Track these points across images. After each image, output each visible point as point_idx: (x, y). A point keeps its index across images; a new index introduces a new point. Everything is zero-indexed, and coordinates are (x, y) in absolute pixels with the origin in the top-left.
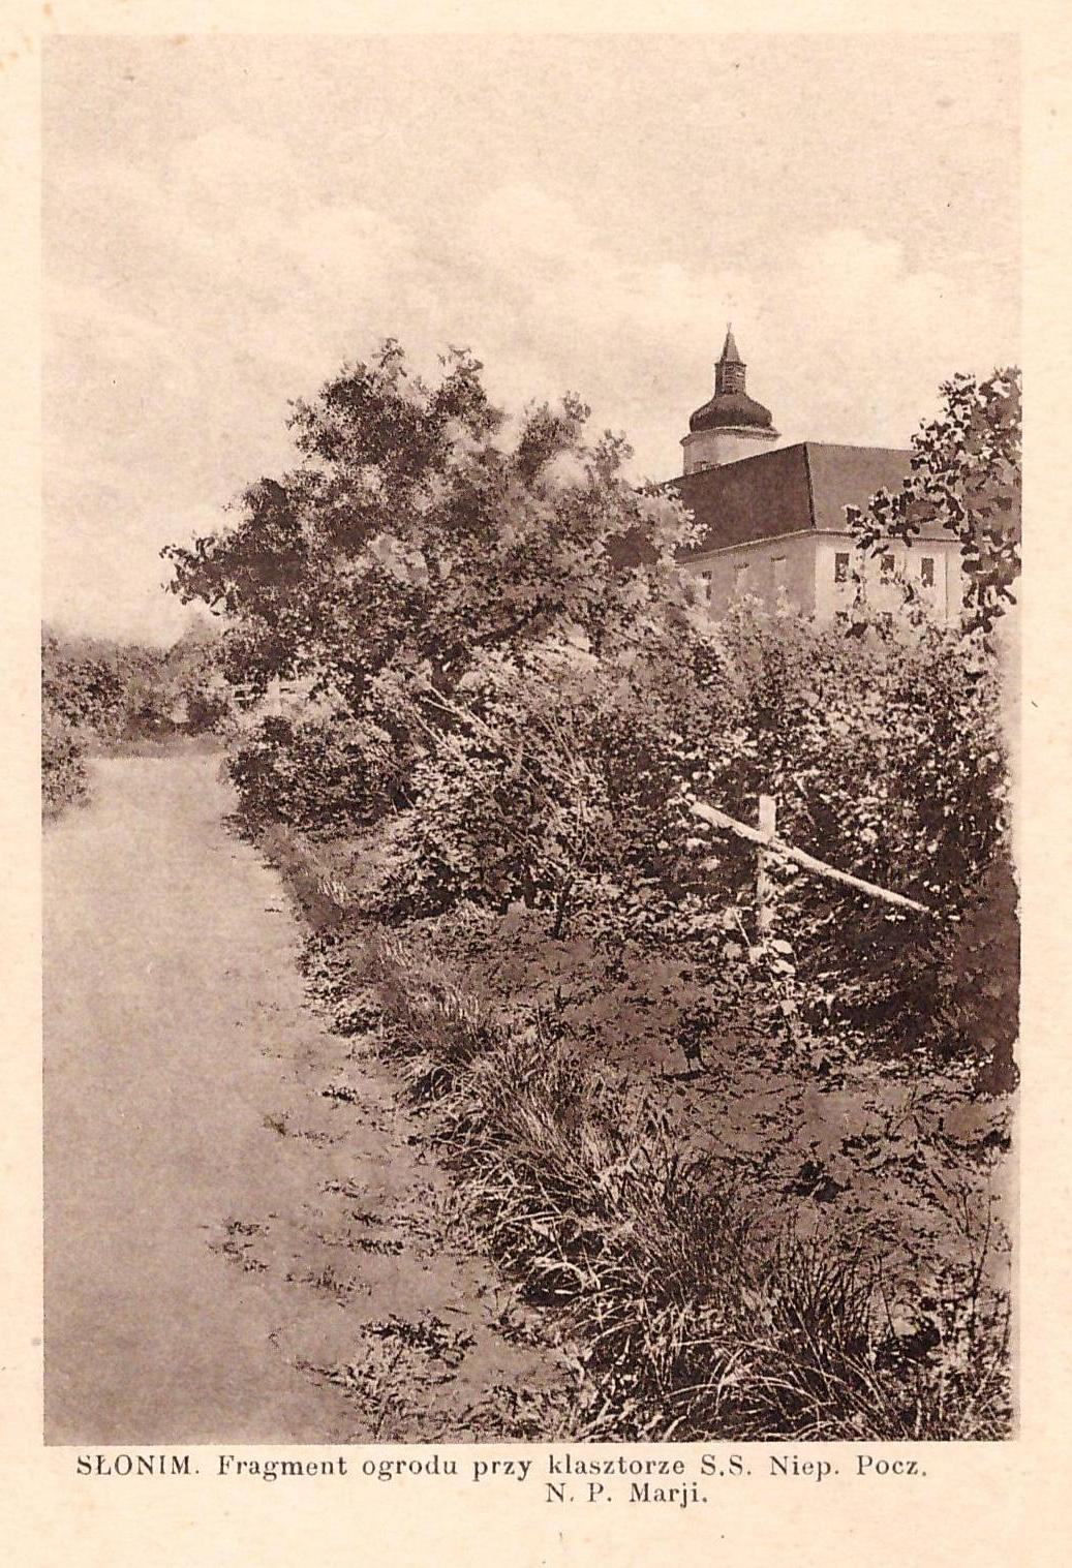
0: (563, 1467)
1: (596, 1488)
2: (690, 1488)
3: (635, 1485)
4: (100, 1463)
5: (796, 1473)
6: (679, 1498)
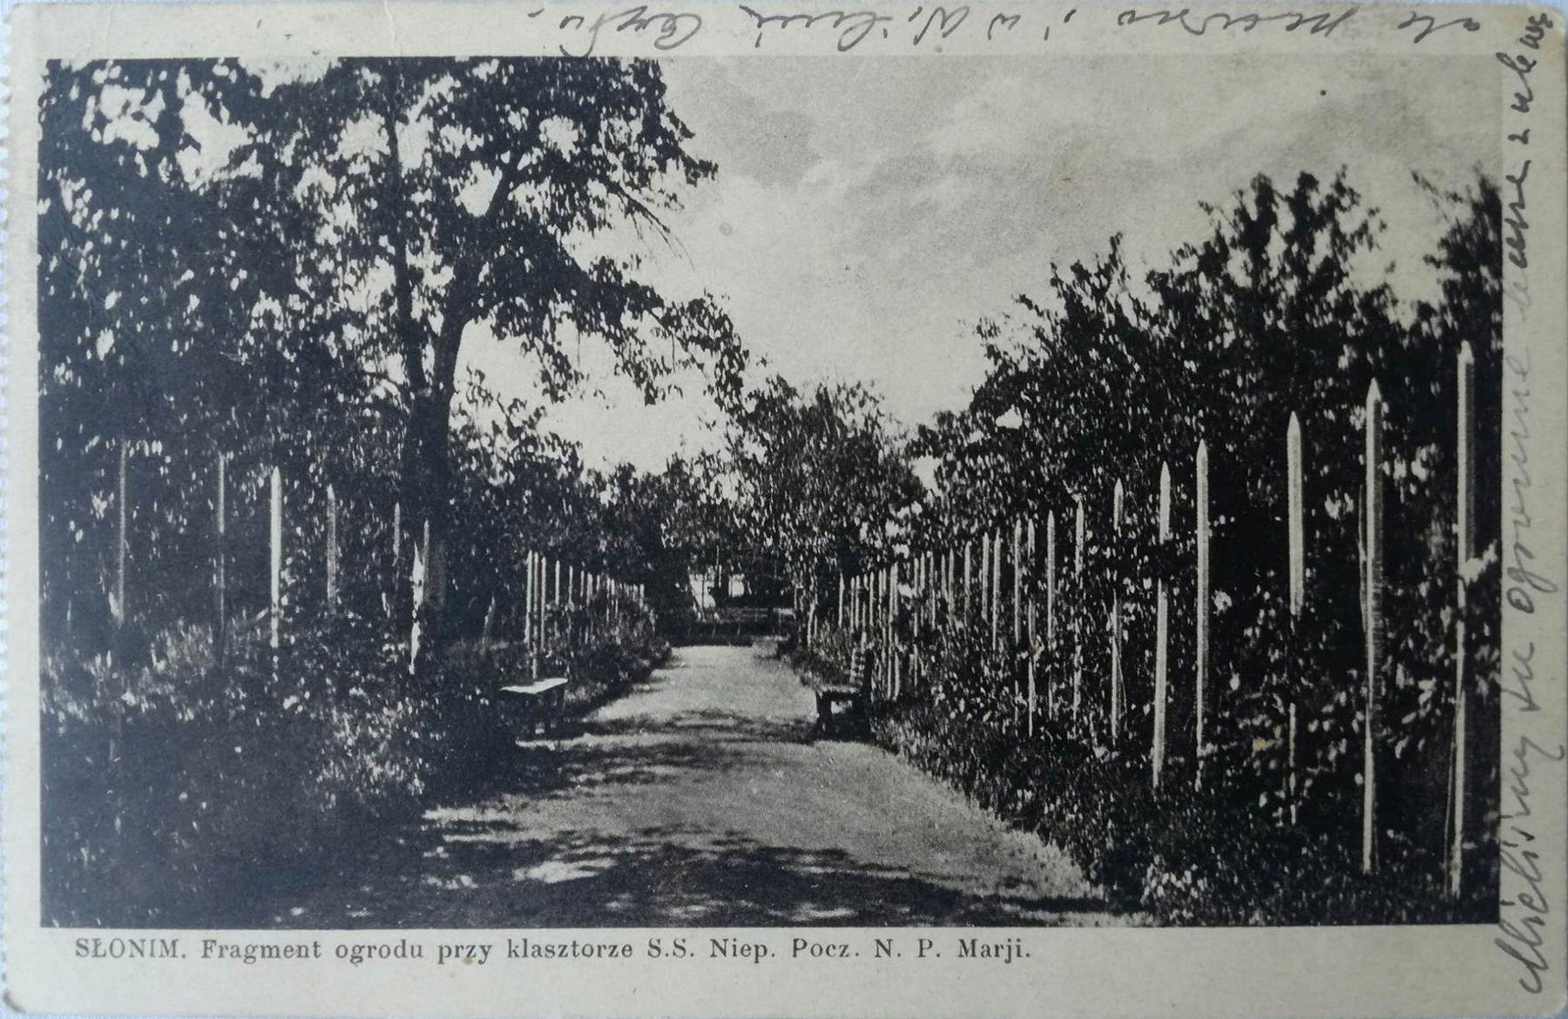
0: (520, 951)
1: (926, 944)
2: (1014, 944)
3: (962, 941)
5: (735, 955)
6: (1004, 953)
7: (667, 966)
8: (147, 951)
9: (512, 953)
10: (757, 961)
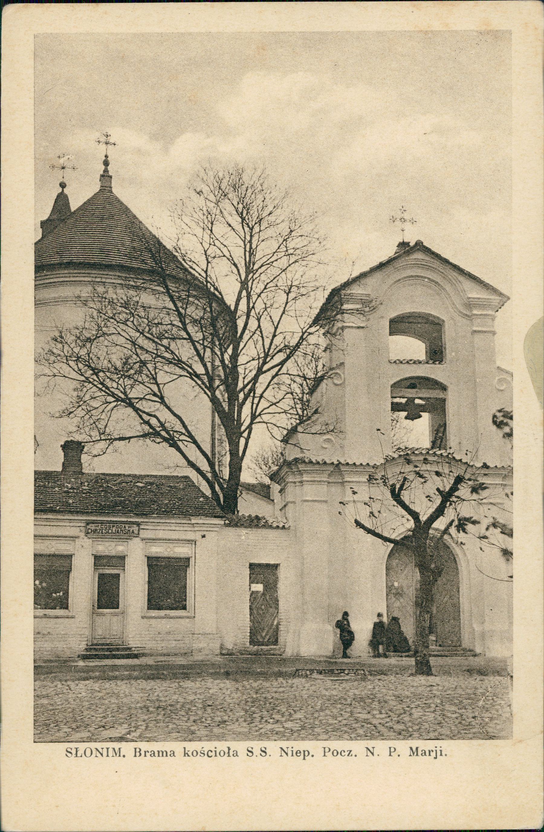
1: (392, 750)
2: (438, 749)
4: (77, 752)
5: (292, 755)
7: (258, 761)
8: (105, 754)
9: (186, 754)
10: (304, 759)
